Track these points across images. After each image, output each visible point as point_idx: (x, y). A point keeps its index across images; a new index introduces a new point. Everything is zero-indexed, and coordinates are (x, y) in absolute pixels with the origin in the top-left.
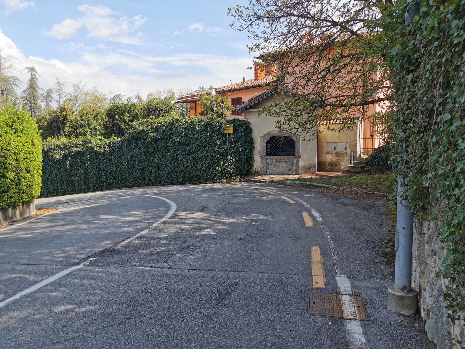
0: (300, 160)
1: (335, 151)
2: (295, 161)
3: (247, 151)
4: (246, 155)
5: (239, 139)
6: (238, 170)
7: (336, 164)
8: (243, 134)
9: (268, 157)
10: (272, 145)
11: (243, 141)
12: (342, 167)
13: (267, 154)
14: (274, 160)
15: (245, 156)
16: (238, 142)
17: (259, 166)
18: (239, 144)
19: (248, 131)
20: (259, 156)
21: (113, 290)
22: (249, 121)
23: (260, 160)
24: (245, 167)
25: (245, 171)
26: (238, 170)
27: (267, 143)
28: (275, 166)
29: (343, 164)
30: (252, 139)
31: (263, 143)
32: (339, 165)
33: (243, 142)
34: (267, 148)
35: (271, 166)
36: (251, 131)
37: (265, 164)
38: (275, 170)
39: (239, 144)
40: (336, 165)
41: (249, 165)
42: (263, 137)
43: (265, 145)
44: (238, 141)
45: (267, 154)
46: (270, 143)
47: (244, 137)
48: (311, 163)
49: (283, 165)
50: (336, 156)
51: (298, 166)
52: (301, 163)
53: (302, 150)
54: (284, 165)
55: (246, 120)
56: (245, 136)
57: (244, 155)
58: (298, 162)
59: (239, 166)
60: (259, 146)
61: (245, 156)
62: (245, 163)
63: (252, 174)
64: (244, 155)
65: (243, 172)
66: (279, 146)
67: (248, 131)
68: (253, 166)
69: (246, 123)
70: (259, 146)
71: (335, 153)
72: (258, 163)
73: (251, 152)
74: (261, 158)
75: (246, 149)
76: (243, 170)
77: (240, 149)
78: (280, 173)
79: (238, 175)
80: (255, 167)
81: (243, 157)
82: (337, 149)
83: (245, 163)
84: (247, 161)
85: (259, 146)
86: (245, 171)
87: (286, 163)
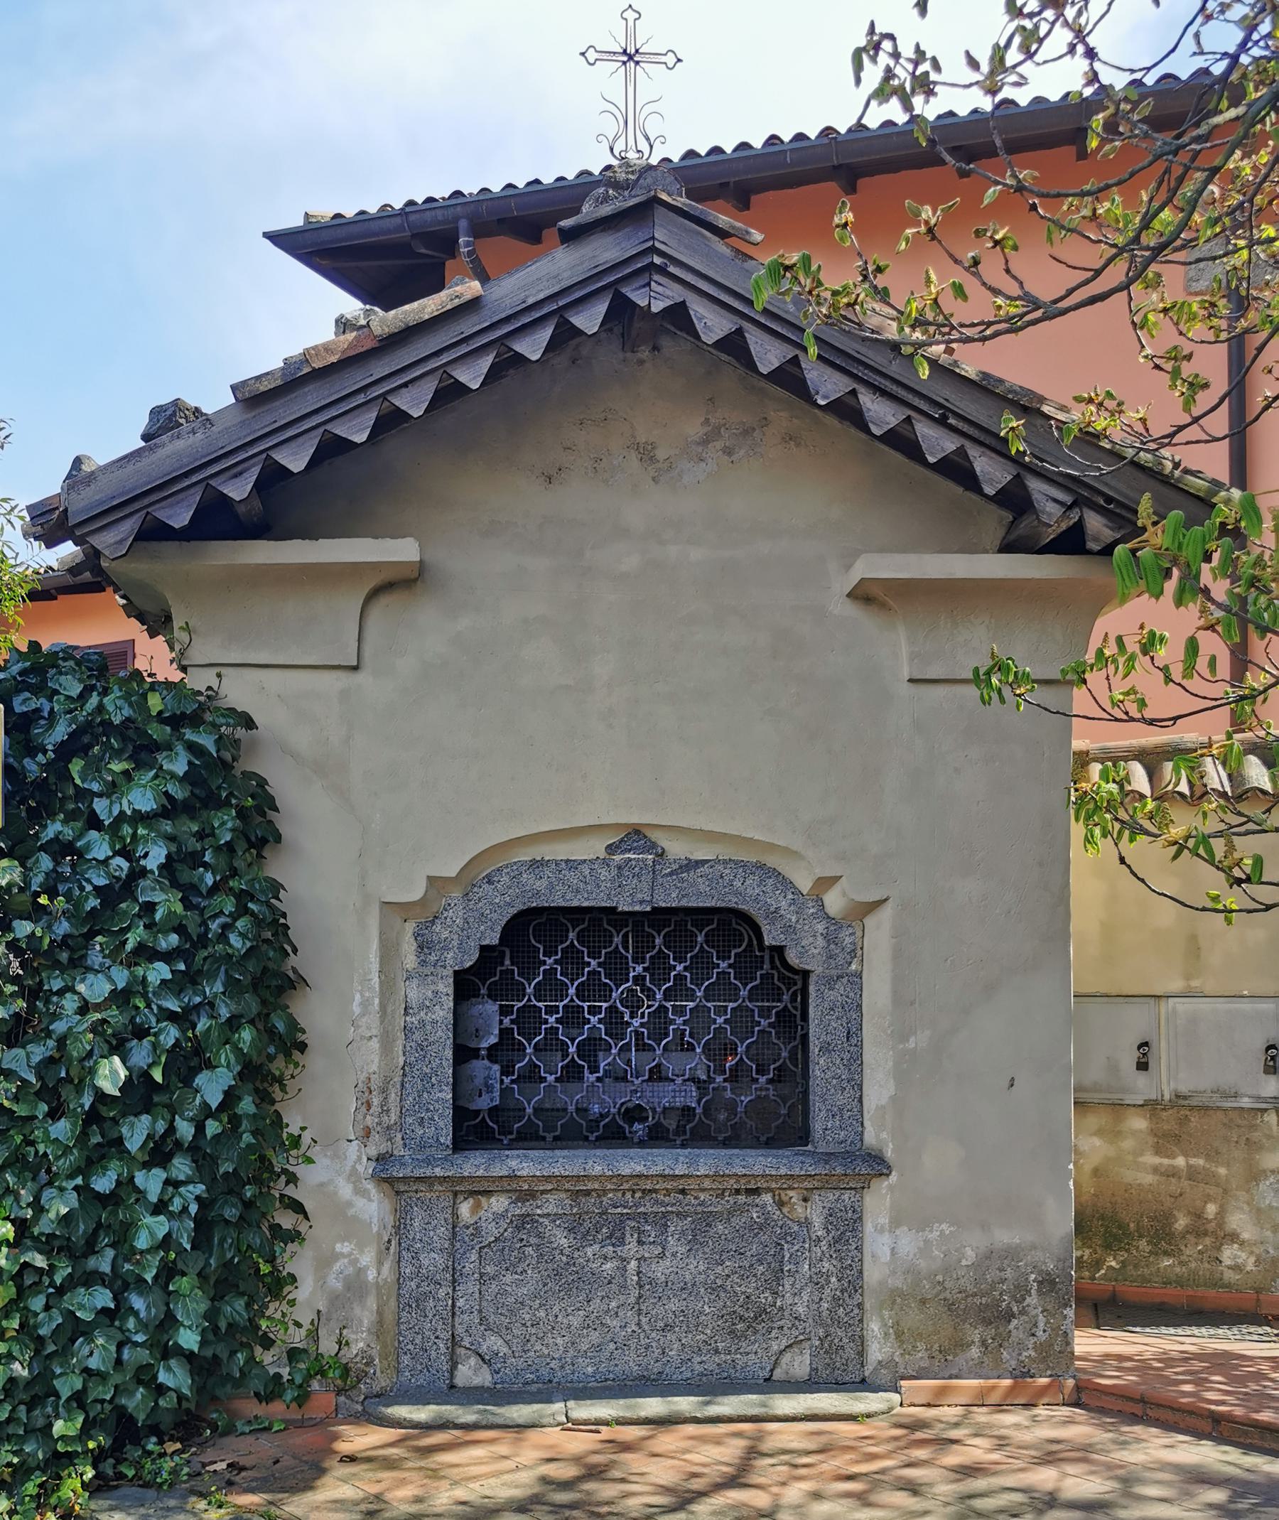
0: (878, 1204)
1: (1143, 1087)
2: (815, 1213)
3: (212, 1086)
4: (194, 1150)
5: (93, 924)
6: (67, 1386)
7: (1168, 1217)
8: (156, 856)
9: (474, 1164)
10: (528, 1020)
11: (146, 953)
12: (1229, 1254)
13: (473, 1130)
14: (551, 1204)
15: (181, 1167)
16: (78, 964)
17: (355, 1287)
18: (95, 988)
19: (225, 825)
20: (357, 1156)
21: (103, 1298)
22: (238, 692)
23: (373, 1208)
24: (169, 1322)
25: (174, 1377)
26: (67, 1386)
27: (466, 986)
28: (569, 1279)
29: (1238, 1220)
30: (274, 931)
31: (414, 993)
32: (1199, 1229)
33: (159, 972)
34: (463, 1054)
35: (522, 1285)
36: (260, 828)
37: (433, 1260)
38: (565, 1334)
39: (95, 988)
40: (1162, 1236)
41: (221, 1285)
42: (424, 917)
43: (444, 1011)
44: (72, 957)
45: (473, 1130)
46: (505, 990)
47: (167, 902)
48: (1005, 1237)
49: (660, 1270)
50: (1164, 1141)
51: (853, 1283)
52: (888, 1247)
53: (901, 1076)
54: (675, 1261)
55: (199, 681)
56: (189, 893)
57: (159, 1152)
58: (847, 1229)
59: (75, 1329)
60: (367, 1022)
61: (181, 1167)
62: (168, 1272)
63: (272, 1389)
64: (159, 1152)
65: (137, 1402)
66: (614, 1021)
67: (225, 825)
68: (279, 1284)
69: (195, 720)
70: (367, 1022)
71: (1152, 1107)
72: (345, 1246)
73: (264, 1098)
74: (385, 1173)
75: (188, 1061)
76: (145, 1376)
77: (111, 1075)
78: (631, 1363)
79: (59, 1462)
80: (308, 1294)
81: (151, 1182)
82: (1162, 1055)
83: (168, 1272)
84: (204, 1227)
85: (371, 1024)
86: (174, 1377)
87: (694, 1242)
